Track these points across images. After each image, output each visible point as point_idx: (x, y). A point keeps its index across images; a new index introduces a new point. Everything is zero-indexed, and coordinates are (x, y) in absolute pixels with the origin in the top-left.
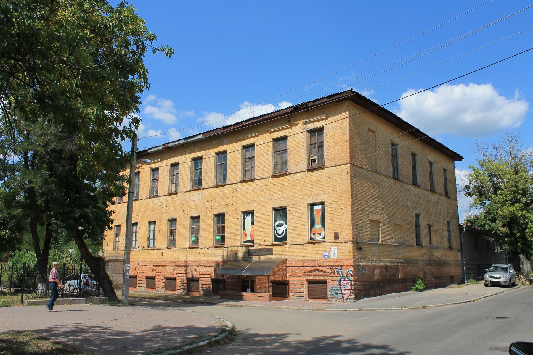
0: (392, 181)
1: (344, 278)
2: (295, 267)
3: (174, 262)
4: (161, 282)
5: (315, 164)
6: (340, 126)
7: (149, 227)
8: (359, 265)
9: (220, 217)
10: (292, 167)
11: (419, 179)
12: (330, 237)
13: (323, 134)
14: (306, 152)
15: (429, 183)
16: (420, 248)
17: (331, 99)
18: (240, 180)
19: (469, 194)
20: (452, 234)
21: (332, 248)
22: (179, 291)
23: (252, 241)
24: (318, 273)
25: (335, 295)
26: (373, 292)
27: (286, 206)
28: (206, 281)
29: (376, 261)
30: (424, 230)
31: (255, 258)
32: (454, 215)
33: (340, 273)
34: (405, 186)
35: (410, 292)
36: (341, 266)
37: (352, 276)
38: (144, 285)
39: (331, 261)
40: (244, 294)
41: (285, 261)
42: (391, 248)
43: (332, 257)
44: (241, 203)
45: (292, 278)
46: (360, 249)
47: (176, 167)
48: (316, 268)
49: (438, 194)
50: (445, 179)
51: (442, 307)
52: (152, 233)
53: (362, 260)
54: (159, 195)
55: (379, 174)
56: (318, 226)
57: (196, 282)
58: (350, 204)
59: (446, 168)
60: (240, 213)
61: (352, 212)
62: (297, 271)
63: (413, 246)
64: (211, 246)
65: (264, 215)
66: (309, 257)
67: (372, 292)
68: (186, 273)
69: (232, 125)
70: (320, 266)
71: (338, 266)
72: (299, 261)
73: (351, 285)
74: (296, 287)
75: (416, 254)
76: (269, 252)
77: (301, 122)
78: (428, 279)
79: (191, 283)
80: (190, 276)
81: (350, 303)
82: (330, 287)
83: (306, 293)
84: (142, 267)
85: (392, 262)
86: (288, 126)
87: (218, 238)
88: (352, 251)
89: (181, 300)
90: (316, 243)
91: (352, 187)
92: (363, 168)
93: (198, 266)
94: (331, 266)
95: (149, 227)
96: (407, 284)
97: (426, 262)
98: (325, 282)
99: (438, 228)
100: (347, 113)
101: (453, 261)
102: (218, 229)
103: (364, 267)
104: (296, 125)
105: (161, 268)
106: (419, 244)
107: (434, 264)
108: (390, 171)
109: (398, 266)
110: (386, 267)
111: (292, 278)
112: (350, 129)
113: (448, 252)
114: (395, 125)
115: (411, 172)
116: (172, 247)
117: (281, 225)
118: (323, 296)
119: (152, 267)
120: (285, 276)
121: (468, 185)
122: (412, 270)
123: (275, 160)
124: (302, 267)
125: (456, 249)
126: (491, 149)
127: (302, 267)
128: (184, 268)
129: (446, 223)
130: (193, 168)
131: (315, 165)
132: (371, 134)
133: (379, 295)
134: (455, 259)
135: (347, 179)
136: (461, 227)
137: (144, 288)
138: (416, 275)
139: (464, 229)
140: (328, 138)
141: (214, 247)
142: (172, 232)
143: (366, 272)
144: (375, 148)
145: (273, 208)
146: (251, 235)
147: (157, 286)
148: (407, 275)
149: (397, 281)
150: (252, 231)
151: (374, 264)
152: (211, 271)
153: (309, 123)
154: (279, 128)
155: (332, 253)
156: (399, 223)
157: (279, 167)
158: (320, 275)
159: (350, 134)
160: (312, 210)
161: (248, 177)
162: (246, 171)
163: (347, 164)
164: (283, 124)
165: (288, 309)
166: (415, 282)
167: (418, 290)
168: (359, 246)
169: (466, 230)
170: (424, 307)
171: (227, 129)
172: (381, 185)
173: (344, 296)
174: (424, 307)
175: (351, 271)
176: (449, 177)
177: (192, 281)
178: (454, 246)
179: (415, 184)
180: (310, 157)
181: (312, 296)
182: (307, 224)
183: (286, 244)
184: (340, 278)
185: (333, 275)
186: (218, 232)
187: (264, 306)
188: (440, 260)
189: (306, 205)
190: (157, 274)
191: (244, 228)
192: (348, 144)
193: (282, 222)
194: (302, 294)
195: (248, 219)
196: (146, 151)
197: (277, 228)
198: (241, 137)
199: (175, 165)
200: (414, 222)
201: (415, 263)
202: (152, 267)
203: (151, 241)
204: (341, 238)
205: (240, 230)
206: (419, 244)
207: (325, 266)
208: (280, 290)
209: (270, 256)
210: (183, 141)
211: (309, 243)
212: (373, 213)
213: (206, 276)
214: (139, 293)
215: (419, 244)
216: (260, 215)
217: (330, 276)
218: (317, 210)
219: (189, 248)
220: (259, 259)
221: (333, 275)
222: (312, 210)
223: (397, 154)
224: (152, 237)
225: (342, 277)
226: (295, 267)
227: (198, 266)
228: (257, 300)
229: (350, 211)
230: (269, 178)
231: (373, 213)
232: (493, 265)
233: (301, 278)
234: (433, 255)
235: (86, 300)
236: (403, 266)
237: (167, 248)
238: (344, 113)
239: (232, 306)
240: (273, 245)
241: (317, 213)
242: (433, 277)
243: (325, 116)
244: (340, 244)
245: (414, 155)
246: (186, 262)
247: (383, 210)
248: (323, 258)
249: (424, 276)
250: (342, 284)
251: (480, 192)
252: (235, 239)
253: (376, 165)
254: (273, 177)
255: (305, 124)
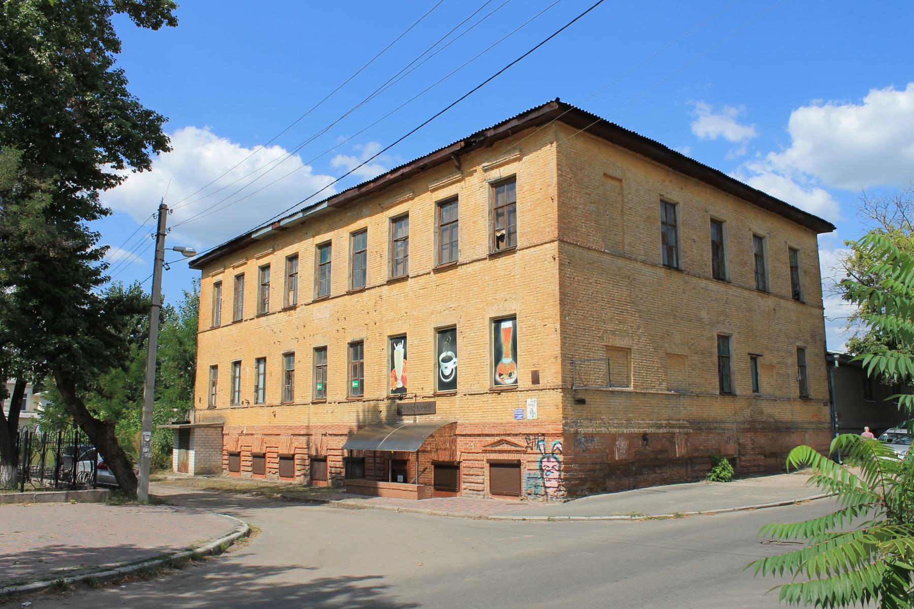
0: (662, 272)
1: (548, 458)
2: (470, 435)
3: (290, 428)
4: (273, 464)
5: (503, 244)
6: (542, 171)
7: (258, 367)
8: (577, 433)
9: (357, 346)
10: (465, 253)
11: (730, 269)
12: (525, 382)
13: (514, 188)
14: (487, 223)
15: (753, 275)
16: (727, 399)
17: (524, 120)
18: (387, 279)
19: (849, 297)
20: (809, 371)
21: (529, 401)
22: (299, 479)
23: (403, 390)
24: (506, 447)
25: (533, 489)
26: (613, 483)
27: (455, 325)
28: (335, 463)
29: (618, 425)
30: (739, 366)
31: (408, 421)
32: (813, 336)
33: (542, 448)
34: (695, 280)
35: (703, 482)
36: (543, 435)
37: (561, 453)
38: (250, 469)
39: (526, 425)
40: (381, 484)
41: (454, 425)
42: (650, 397)
43: (529, 417)
44: (387, 321)
45: (465, 456)
46: (582, 402)
47: (294, 262)
48: (503, 437)
49: (775, 296)
50: (794, 268)
51: (716, 516)
52: (261, 377)
53: (586, 423)
54: (271, 312)
55: (630, 259)
56: (507, 360)
57: (322, 464)
58: (558, 317)
59: (795, 246)
60: (386, 338)
61: (563, 332)
62: (476, 444)
63: (712, 396)
64: (343, 399)
65: (423, 341)
66: (491, 419)
67: (610, 483)
68: (308, 448)
69: (370, 182)
70: (509, 435)
71: (537, 434)
72: (476, 425)
73: (559, 470)
74: (471, 473)
75: (719, 410)
76: (429, 408)
77: (479, 168)
78: (748, 457)
79: (316, 463)
80: (313, 453)
81: (558, 504)
82: (525, 473)
83: (487, 483)
84: (246, 437)
85: (660, 427)
86: (458, 176)
87: (355, 384)
88: (560, 405)
89: (279, 495)
90: (502, 391)
91: (562, 285)
92: (589, 249)
93: (325, 435)
94: (528, 435)
95: (258, 367)
96: (697, 467)
97: (742, 426)
98: (517, 465)
99: (775, 361)
100: (555, 144)
101: (811, 423)
102: (355, 368)
103: (590, 437)
104: (471, 174)
105: (273, 438)
106: (726, 390)
107: (763, 428)
108: (658, 253)
109: (673, 434)
110: (645, 437)
111: (465, 456)
112: (559, 176)
113: (798, 406)
114: (670, 166)
115: (708, 255)
116: (289, 401)
117: (447, 360)
118: (514, 490)
119: (260, 436)
120: (453, 453)
121: (846, 277)
122: (710, 442)
123: (441, 241)
124: (479, 435)
125: (818, 401)
126: (892, 207)
127: (479, 435)
128: (304, 439)
129: (795, 351)
130: (318, 263)
131: (503, 246)
132: (610, 183)
133: (629, 489)
134: (815, 419)
135: (552, 270)
136: (829, 359)
137: (251, 474)
138: (719, 450)
139: (836, 362)
140: (523, 195)
141: (349, 401)
142: (289, 376)
143: (596, 445)
144: (622, 211)
145: (435, 329)
146: (404, 379)
147: (268, 470)
148: (696, 450)
149: (673, 462)
150: (404, 370)
151: (613, 430)
152: (341, 442)
153: (492, 168)
154: (445, 181)
155: (529, 409)
156: (677, 351)
157: (446, 253)
158: (509, 452)
159: (560, 184)
160: (497, 330)
161: (400, 274)
162: (397, 263)
163: (553, 241)
164: (452, 173)
165: (432, 514)
166: (715, 464)
167: (719, 478)
168: (579, 396)
169: (839, 364)
170: (678, 516)
171: (364, 190)
172: (635, 279)
173: (548, 490)
174: (678, 516)
175: (557, 443)
176: (803, 262)
177: (317, 460)
178: (812, 393)
179: (719, 275)
180: (495, 231)
181: (496, 491)
182: (488, 355)
183: (455, 394)
184: (541, 456)
185: (529, 450)
186: (355, 375)
187: (396, 508)
188: (776, 422)
189: (487, 322)
190: (268, 450)
191: (393, 367)
192: (556, 203)
193: (450, 353)
194: (480, 487)
195: (399, 348)
196: (250, 234)
197: (443, 365)
198: (387, 203)
199: (293, 258)
200: (716, 351)
201: (715, 428)
202: (260, 436)
203: (261, 392)
204: (543, 382)
205: (385, 370)
206: (726, 390)
207: (516, 435)
208: (446, 477)
209: (431, 417)
210: (301, 215)
211: (492, 391)
212: (613, 333)
213: (336, 453)
214: (241, 482)
215: (726, 390)
216: (416, 342)
217: (525, 452)
218: (507, 330)
219: (313, 403)
220: (415, 421)
221: (529, 450)
222: (497, 330)
223: (675, 221)
224: (261, 386)
225: (545, 455)
226: (470, 435)
227: (325, 435)
228: (400, 497)
229: (559, 330)
230: (429, 273)
231: (613, 333)
232: (888, 431)
233: (479, 456)
234: (762, 413)
235: (67, 495)
236: (686, 434)
237: (282, 404)
238: (549, 146)
239: (353, 507)
240: (436, 395)
241: (506, 336)
242: (760, 454)
243: (517, 154)
244: (541, 393)
245: (717, 224)
246: (308, 427)
247: (639, 328)
248: (513, 420)
249: (740, 451)
250: (545, 468)
251: (864, 291)
252: (378, 388)
253: (623, 242)
254: (437, 271)
255: (485, 171)
